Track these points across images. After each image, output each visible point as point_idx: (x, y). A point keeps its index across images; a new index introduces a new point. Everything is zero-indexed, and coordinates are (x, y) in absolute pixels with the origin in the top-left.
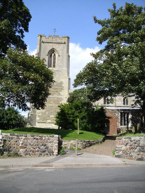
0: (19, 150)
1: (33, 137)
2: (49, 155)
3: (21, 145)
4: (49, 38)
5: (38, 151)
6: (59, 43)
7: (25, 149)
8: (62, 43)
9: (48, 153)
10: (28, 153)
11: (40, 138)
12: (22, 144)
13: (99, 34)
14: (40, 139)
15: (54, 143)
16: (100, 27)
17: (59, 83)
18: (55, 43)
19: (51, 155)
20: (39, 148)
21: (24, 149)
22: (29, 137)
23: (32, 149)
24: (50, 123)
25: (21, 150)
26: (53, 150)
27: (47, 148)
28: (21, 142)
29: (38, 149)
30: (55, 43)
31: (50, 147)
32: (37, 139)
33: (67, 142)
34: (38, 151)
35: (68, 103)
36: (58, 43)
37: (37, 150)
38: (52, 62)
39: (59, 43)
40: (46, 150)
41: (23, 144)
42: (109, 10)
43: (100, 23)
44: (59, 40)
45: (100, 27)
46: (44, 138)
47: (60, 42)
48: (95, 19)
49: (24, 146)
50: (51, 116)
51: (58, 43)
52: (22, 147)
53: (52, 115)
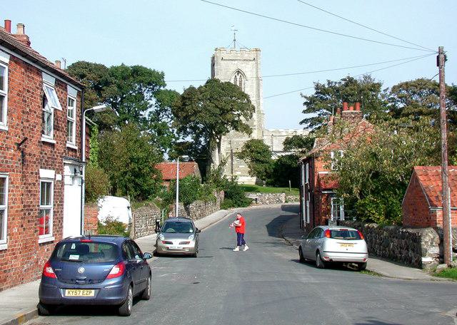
18: (240, 60)
30: (240, 60)
43: (306, 97)
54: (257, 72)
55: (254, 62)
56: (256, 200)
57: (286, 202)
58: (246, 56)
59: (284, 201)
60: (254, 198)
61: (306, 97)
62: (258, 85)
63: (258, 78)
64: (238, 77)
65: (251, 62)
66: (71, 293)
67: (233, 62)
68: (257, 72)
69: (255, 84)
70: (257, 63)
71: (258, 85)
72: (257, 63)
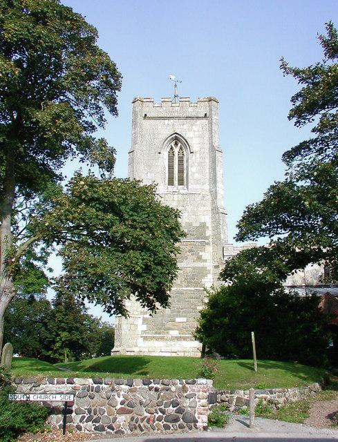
0: (115, 419)
1: (148, 384)
2: (187, 428)
3: (119, 406)
4: (164, 104)
5: (159, 419)
6: (192, 118)
7: (131, 415)
8: (198, 118)
9: (185, 424)
10: (137, 425)
11: (163, 386)
12: (122, 403)
13: (294, 99)
14: (163, 389)
15: (197, 400)
16: (297, 86)
17: (197, 227)
18: (179, 118)
19: (191, 429)
20: (163, 412)
21: (129, 416)
22: (138, 387)
23: (146, 414)
24: (176, 337)
25: (122, 420)
26: (196, 415)
27: (180, 411)
28: (120, 399)
29: (160, 414)
30: (179, 118)
31: (189, 409)
32: (157, 390)
33: (229, 395)
34: (159, 419)
35: (200, 254)
36: (187, 118)
37: (157, 416)
38: (253, 341)
39: (192, 118)
40: (181, 416)
41: (126, 404)
42: (321, 38)
43: (297, 73)
44: (190, 109)
45: (297, 86)
46: (173, 388)
47: (194, 114)
48: (284, 66)
49: (128, 408)
50: (178, 320)
51: (187, 118)
52: (122, 412)
53: (180, 317)
54: (211, 137)
55: (205, 121)
56: (67, 410)
57: (215, 422)
58: (190, 111)
59: (202, 420)
60: (58, 401)
61: (297, 73)
62: (214, 161)
63: (213, 150)
64: (176, 150)
65: (199, 122)
66: (67, 397)
67: (166, 121)
68: (211, 137)
69: (207, 160)
70: (211, 123)
71: (214, 161)
72: (211, 123)
